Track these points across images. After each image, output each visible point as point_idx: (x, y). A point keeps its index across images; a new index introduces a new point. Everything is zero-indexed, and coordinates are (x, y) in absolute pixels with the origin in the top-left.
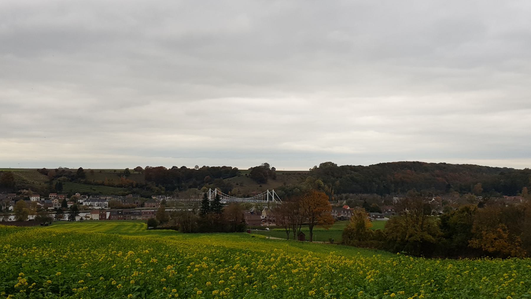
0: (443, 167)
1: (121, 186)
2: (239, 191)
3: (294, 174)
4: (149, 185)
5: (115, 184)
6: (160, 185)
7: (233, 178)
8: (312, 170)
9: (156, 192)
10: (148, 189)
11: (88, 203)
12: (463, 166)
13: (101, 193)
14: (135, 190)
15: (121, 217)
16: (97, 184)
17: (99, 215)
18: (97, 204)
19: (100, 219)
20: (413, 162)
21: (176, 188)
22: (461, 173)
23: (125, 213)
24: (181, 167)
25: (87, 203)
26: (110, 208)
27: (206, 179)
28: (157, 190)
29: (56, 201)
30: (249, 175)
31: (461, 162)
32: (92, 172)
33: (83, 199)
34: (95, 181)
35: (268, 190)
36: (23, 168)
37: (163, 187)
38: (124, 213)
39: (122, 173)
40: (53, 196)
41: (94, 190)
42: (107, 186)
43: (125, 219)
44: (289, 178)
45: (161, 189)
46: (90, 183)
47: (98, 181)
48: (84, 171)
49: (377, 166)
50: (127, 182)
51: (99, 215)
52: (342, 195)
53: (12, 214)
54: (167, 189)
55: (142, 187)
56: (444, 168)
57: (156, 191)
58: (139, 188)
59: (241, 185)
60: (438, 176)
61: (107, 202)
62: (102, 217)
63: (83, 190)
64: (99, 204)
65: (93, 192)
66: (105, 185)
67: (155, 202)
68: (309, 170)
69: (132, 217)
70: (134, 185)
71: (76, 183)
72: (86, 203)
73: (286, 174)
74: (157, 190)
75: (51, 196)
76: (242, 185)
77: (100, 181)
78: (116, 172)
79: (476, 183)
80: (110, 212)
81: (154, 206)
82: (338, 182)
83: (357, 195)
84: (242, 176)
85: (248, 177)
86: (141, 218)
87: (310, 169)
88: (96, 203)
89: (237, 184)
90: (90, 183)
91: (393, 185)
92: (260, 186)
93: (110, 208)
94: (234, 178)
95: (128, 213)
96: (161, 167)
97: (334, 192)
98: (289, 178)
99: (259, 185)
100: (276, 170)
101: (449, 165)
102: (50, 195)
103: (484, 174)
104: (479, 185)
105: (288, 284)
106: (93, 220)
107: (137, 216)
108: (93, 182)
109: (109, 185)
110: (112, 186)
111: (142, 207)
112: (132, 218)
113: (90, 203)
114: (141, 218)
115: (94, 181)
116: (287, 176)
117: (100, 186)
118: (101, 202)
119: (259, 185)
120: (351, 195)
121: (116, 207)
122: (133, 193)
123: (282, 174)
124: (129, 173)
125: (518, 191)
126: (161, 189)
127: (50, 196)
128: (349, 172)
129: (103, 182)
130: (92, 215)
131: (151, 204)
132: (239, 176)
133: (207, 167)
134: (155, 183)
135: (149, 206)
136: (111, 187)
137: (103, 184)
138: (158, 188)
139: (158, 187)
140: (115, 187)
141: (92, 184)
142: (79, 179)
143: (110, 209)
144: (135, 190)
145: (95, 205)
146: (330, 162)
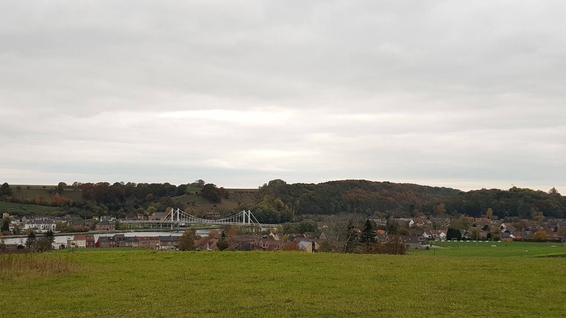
0: (387, 185)
1: (55, 205)
2: (192, 212)
3: (247, 193)
4: (88, 204)
5: (47, 203)
6: (102, 205)
7: (181, 196)
8: (261, 188)
9: (98, 213)
10: (88, 208)
11: (32, 226)
12: (404, 185)
13: (33, 213)
14: (72, 209)
16: (27, 203)
17: (85, 241)
18: (43, 227)
19: (87, 246)
20: (360, 180)
21: (120, 208)
22: (407, 193)
23: (118, 239)
24: (114, 184)
25: (31, 225)
26: (60, 232)
27: (148, 198)
28: (99, 210)
30: (200, 192)
31: (403, 182)
32: (19, 188)
33: (16, 220)
34: (24, 199)
35: (244, 211)
37: (105, 207)
38: (117, 239)
39: (54, 190)
41: (24, 209)
42: (39, 204)
43: (118, 246)
44: (242, 197)
45: (104, 209)
46: (17, 202)
47: (28, 199)
48: (9, 187)
49: (328, 185)
50: (62, 200)
51: (86, 242)
52: (302, 216)
54: (110, 209)
55: (80, 206)
56: (390, 187)
57: (98, 211)
58: (76, 207)
59: (193, 204)
60: (386, 195)
61: (54, 225)
62: (89, 243)
63: (11, 209)
64: (46, 226)
65: (24, 211)
66: (36, 204)
67: (109, 224)
68: (258, 188)
69: (126, 243)
70: (71, 204)
72: (29, 225)
73: (238, 192)
74: (99, 210)
76: (194, 204)
77: (30, 199)
78: (45, 189)
79: (439, 204)
80: (74, 236)
81: (108, 229)
82: (298, 202)
83: (316, 216)
84: (192, 194)
85: (198, 195)
86: (137, 245)
87: (259, 187)
88: (41, 225)
89: (189, 204)
90: (17, 202)
91: (349, 205)
92: (215, 206)
93: (60, 232)
94: (182, 197)
95: (122, 239)
96: (212, 185)
97: (295, 212)
98: (242, 197)
99: (213, 205)
100: (177, 186)
101: (393, 184)
103: (427, 194)
104: (442, 205)
106: (79, 247)
107: (132, 243)
108: (22, 200)
109: (41, 204)
110: (45, 205)
111: (93, 230)
112: (127, 245)
113: (34, 225)
114: (137, 245)
115: (23, 199)
116: (240, 195)
117: (31, 205)
118: (37, 224)
119: (213, 205)
120: (311, 215)
121: (65, 231)
122: (71, 213)
123: (234, 192)
124: (61, 190)
125: (482, 213)
126: (104, 209)
128: (305, 191)
129: (34, 200)
130: (78, 241)
131: (104, 226)
132: (188, 195)
133: (133, 183)
134: (95, 202)
135: (102, 229)
136: (43, 207)
137: (34, 203)
138: (100, 208)
139: (99, 206)
141: (21, 203)
142: (4, 196)
143: (60, 233)
144: (72, 209)
145: (40, 228)
146: (280, 180)
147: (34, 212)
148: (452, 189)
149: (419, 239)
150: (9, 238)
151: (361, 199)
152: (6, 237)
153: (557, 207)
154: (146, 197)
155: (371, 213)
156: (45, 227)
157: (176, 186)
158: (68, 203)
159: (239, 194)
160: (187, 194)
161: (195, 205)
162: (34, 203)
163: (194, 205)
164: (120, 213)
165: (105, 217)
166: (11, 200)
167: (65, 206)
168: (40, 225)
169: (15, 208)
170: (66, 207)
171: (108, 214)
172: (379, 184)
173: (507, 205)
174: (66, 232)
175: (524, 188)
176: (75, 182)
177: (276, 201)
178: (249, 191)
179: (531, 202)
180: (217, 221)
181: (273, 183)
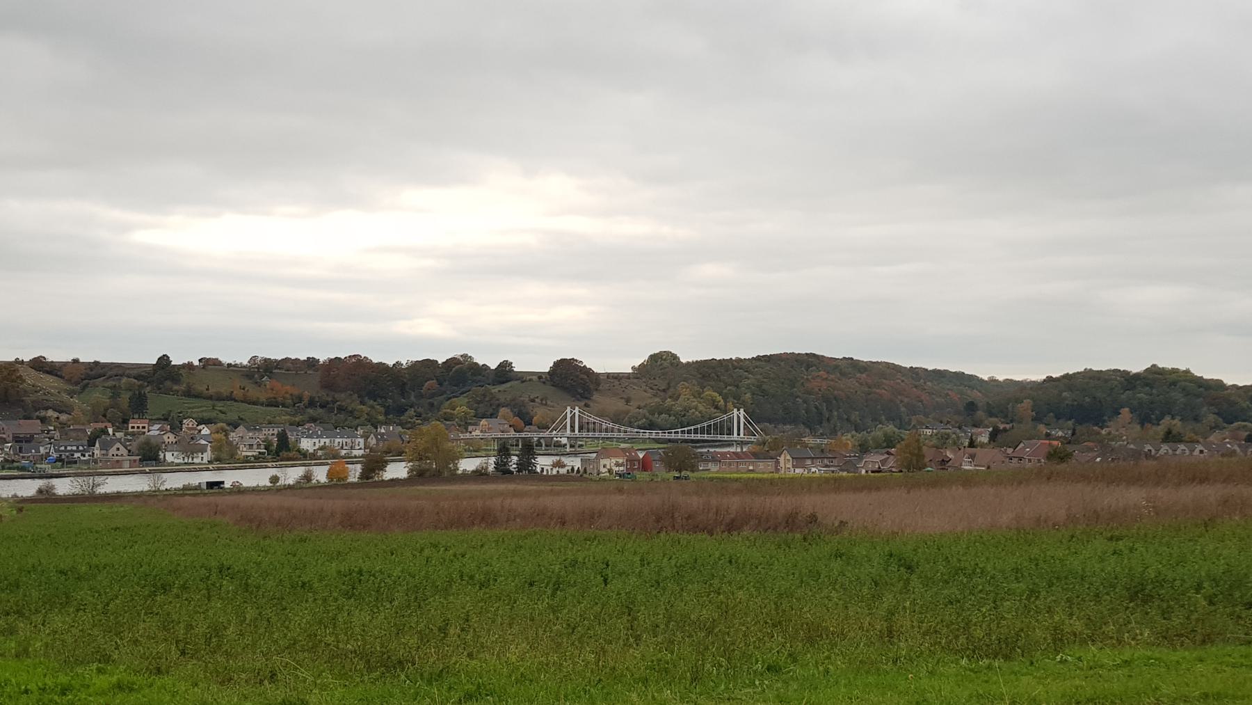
0: (852, 366)
10: (341, 409)
11: (319, 442)
13: (242, 419)
15: (742, 449)
16: (220, 398)
18: (339, 445)
21: (407, 410)
25: (317, 441)
29: (169, 438)
36: (146, 363)
40: (141, 425)
53: (148, 471)
71: (166, 394)
72: (314, 440)
75: (136, 425)
76: (544, 402)
77: (225, 390)
84: (530, 380)
90: (198, 396)
95: (693, 456)
99: (583, 404)
102: (130, 425)
104: (1027, 403)
105: (1024, 587)
115: (208, 389)
118: (348, 437)
127: (133, 427)
132: (523, 382)
137: (230, 398)
140: (262, 405)
147: (243, 417)
148: (429, 364)
149: (551, 473)
150: (293, 466)
151: (840, 392)
152: (246, 466)
153: (1248, 406)
154: (424, 388)
155: (859, 421)
156: (342, 444)
157: (437, 361)
158: (300, 399)
159: (617, 383)
160: (519, 381)
161: (546, 402)
162: (230, 398)
163: (546, 404)
164: (410, 420)
165: (391, 427)
166: (184, 392)
167: (296, 405)
168: (334, 441)
169: (203, 407)
170: (298, 407)
171: (386, 422)
172: (1119, 374)
173: (1152, 403)
174: (391, 454)
175: (1173, 367)
176: (254, 355)
177: (707, 395)
178: (135, 372)
179: (1198, 396)
180: (668, 433)
181: (654, 358)
